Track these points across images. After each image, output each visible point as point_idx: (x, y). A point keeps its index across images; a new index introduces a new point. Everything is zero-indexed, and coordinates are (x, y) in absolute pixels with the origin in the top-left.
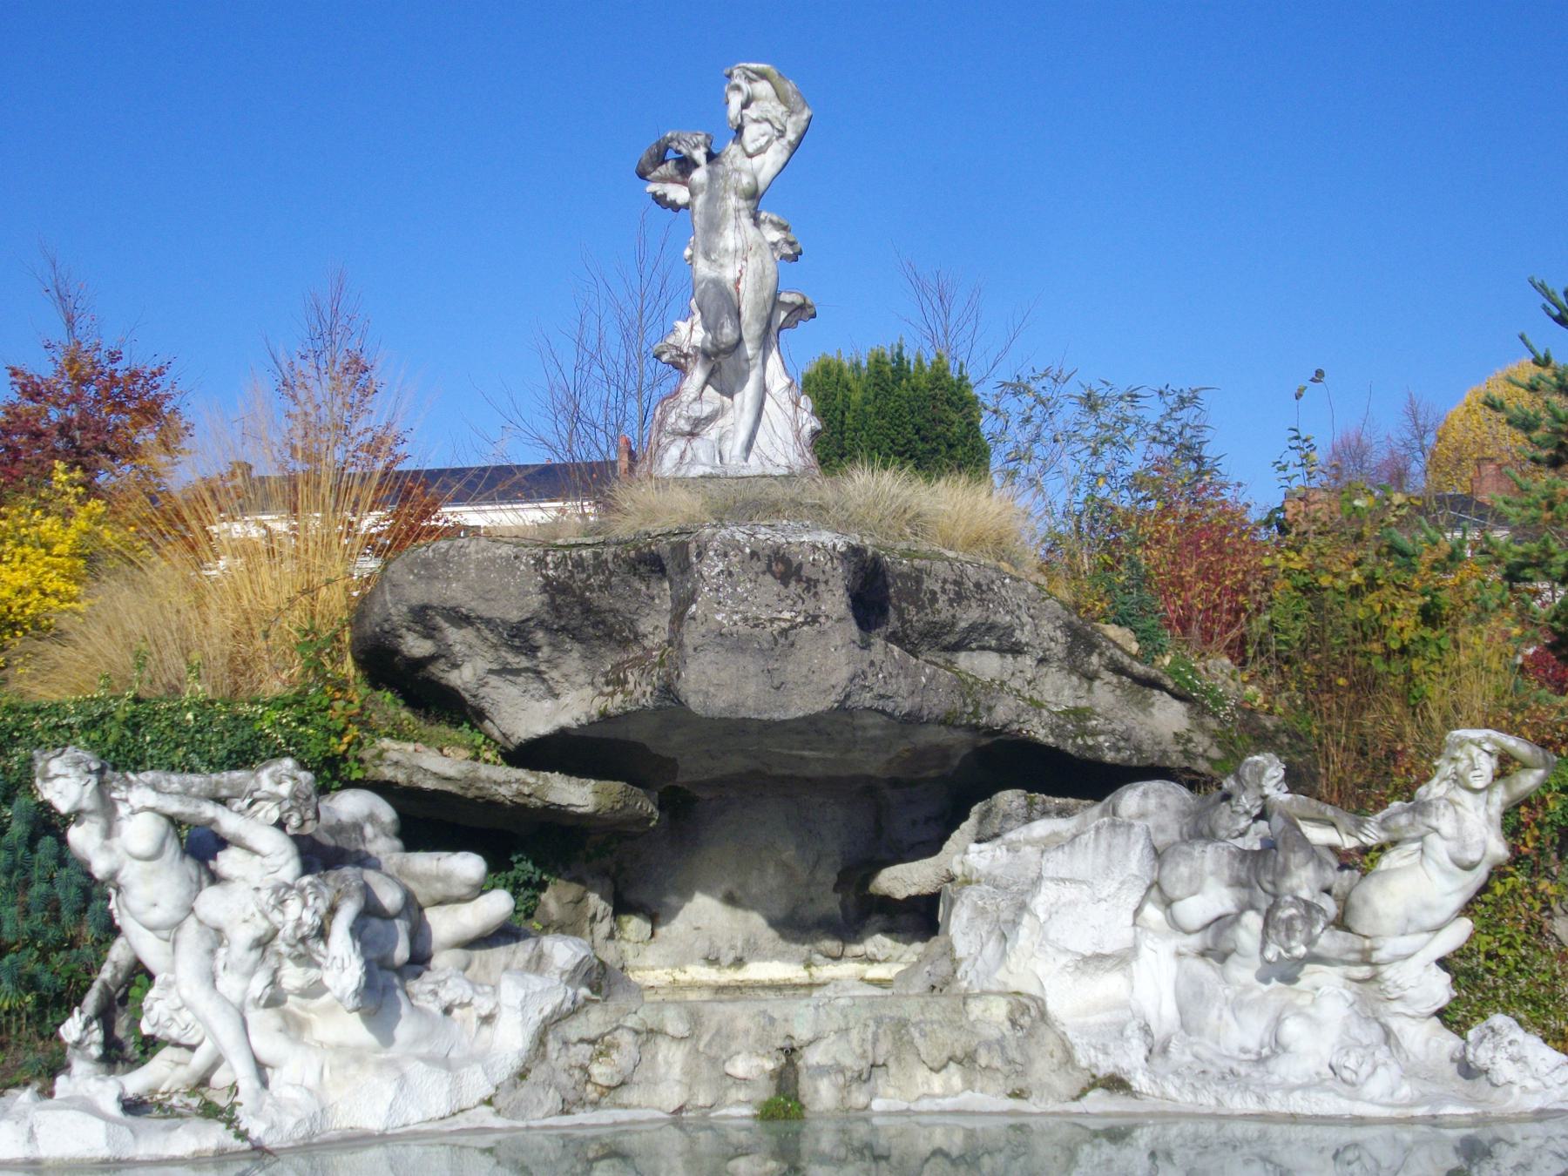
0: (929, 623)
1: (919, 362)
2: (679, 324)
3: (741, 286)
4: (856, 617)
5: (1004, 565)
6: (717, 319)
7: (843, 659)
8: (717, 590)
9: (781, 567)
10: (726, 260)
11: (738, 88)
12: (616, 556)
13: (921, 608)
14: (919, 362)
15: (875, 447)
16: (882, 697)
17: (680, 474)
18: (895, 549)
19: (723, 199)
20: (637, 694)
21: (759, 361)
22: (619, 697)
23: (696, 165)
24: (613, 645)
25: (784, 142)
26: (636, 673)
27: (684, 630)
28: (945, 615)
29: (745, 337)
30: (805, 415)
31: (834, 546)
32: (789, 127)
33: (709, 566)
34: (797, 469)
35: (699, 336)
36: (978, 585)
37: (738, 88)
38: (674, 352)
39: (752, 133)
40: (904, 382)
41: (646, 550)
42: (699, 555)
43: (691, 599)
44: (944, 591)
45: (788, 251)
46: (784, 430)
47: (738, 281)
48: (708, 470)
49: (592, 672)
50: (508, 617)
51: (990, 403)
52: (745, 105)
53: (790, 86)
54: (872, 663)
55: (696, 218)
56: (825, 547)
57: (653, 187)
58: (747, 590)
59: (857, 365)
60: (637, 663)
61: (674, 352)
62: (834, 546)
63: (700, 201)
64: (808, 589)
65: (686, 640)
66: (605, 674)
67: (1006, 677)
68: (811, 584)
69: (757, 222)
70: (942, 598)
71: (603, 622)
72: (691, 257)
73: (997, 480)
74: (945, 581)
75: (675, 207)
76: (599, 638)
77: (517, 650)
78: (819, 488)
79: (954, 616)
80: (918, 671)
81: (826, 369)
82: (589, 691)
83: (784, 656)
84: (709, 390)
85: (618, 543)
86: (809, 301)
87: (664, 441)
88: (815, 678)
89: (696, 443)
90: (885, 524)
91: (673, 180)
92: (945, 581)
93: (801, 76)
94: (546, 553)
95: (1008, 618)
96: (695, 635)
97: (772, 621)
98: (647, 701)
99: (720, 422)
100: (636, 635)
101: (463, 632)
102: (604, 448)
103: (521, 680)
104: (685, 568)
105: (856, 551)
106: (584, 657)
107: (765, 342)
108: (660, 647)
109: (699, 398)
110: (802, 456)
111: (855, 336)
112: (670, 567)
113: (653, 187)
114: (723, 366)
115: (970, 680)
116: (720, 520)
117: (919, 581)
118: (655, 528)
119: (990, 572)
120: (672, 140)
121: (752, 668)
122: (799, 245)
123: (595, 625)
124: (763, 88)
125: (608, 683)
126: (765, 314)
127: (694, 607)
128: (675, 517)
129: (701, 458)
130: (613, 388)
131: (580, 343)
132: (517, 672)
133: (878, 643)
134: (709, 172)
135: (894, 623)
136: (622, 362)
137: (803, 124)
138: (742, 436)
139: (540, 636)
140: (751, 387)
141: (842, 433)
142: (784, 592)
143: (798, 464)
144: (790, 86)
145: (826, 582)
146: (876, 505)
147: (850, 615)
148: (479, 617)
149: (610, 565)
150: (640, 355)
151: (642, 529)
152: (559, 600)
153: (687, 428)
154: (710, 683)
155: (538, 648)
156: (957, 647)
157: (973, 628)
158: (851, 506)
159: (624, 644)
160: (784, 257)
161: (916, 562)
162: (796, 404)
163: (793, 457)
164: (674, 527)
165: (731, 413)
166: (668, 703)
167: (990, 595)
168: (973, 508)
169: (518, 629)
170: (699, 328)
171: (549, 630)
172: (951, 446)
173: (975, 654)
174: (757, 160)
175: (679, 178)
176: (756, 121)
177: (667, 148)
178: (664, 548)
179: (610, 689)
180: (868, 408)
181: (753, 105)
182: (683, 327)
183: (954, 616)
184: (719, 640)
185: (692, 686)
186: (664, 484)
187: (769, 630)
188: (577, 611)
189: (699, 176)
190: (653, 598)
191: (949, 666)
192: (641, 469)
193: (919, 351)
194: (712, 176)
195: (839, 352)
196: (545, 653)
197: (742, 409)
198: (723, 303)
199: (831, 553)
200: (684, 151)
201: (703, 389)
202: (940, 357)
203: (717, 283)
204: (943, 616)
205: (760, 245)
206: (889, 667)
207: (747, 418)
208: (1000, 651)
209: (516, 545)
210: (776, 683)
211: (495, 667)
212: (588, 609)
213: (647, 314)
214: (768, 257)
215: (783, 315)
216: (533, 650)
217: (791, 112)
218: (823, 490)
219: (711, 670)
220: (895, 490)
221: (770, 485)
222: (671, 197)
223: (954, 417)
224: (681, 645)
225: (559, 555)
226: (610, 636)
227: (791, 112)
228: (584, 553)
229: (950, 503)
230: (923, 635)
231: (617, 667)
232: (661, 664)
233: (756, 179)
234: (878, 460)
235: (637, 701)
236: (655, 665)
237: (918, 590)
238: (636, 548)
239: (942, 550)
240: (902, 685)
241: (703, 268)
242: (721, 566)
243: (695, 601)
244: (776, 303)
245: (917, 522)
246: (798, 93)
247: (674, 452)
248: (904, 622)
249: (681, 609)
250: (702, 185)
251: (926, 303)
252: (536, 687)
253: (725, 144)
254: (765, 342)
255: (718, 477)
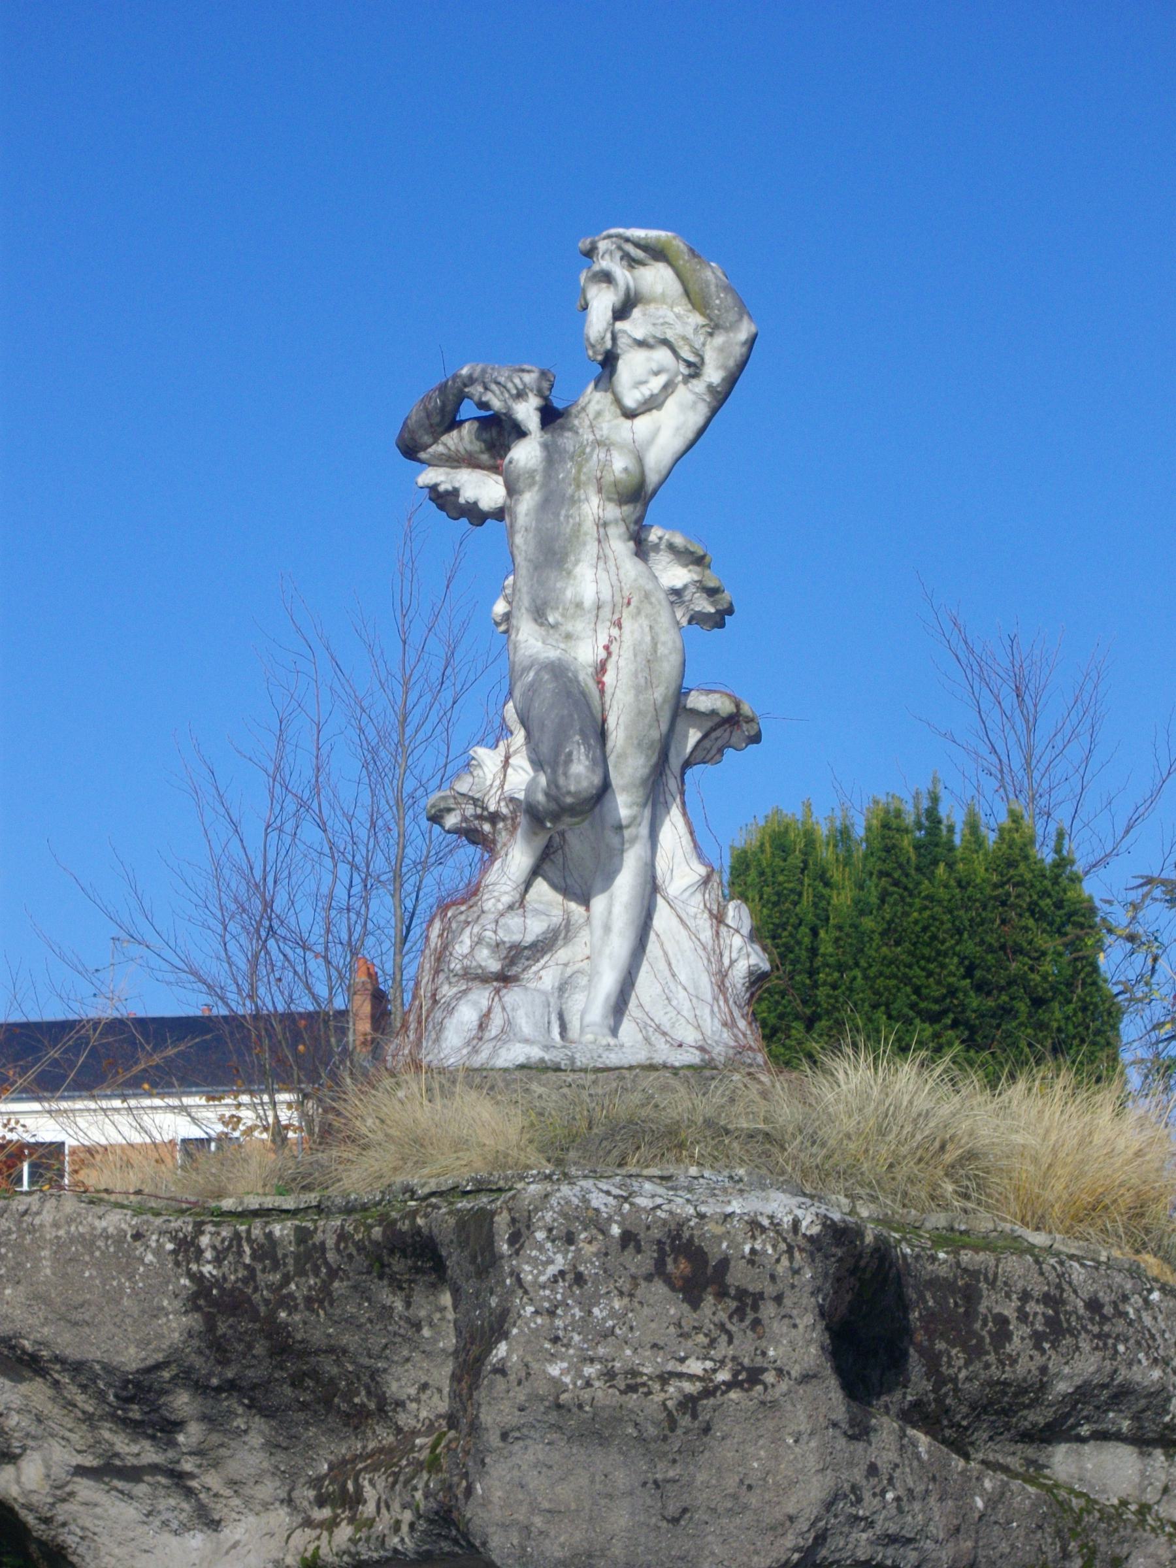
0: (991, 1383)
1: (973, 827)
2: (481, 752)
3: (608, 678)
4: (839, 1371)
5: (1150, 1262)
6: (558, 748)
7: (812, 1462)
8: (552, 1313)
9: (684, 1266)
10: (579, 626)
11: (607, 278)
12: (342, 1236)
13: (975, 1352)
14: (973, 827)
15: (881, 1002)
16: (892, 1539)
17: (478, 1060)
18: (919, 1226)
19: (574, 501)
20: (380, 1527)
21: (644, 830)
22: (344, 1532)
23: (520, 433)
24: (333, 1421)
25: (699, 386)
26: (381, 1483)
27: (481, 1395)
28: (1026, 1367)
29: (616, 780)
30: (737, 941)
31: (796, 1224)
32: (710, 356)
33: (534, 1262)
34: (719, 1053)
35: (521, 777)
36: (1094, 1305)
37: (607, 278)
38: (470, 810)
39: (637, 372)
40: (941, 869)
41: (405, 1226)
42: (514, 1239)
43: (498, 1329)
44: (1023, 1317)
45: (705, 606)
46: (693, 972)
47: (601, 668)
48: (535, 1053)
49: (290, 1477)
50: (117, 1360)
51: (1120, 917)
52: (621, 312)
53: (711, 274)
54: (873, 1470)
55: (519, 540)
56: (776, 1225)
57: (430, 476)
58: (613, 1314)
59: (844, 834)
60: (383, 1460)
61: (470, 810)
62: (796, 1224)
63: (527, 503)
64: (740, 1313)
65: (487, 1417)
66: (315, 1483)
67: (1150, 1496)
68: (747, 1303)
69: (642, 549)
70: (1019, 1333)
71: (314, 1374)
72: (507, 617)
73: (1135, 1078)
74: (1025, 1296)
75: (475, 515)
76: (304, 1406)
77: (136, 1429)
78: (764, 1095)
79: (1043, 1370)
80: (969, 1483)
81: (779, 841)
82: (281, 1517)
83: (690, 1452)
84: (541, 887)
85: (348, 1210)
86: (746, 709)
87: (447, 991)
88: (754, 1500)
89: (513, 996)
90: (901, 1173)
91: (471, 462)
92: (1025, 1296)
93: (735, 265)
94: (199, 1230)
95: (1156, 1374)
96: (506, 1406)
97: (664, 1378)
98: (405, 1542)
99: (562, 954)
100: (382, 1401)
101: (24, 1388)
102: (322, 991)
103: (141, 1489)
104: (486, 1262)
105: (839, 1234)
106: (272, 1447)
107: (656, 790)
108: (430, 1428)
109: (519, 904)
110: (729, 1024)
111: (836, 773)
112: (455, 1260)
113: (430, 476)
114: (570, 837)
115: (1076, 1503)
116: (559, 1162)
117: (971, 1296)
118: (425, 1179)
119: (1118, 1278)
120: (471, 380)
121: (622, 1479)
122: (727, 596)
123: (296, 1382)
124: (657, 278)
125: (321, 1502)
126: (655, 735)
127: (502, 1349)
128: (466, 1156)
129: (521, 1031)
130: (343, 869)
131: (277, 776)
132: (134, 1474)
133: (886, 1427)
134: (545, 446)
135: (918, 1384)
136: (362, 816)
137: (738, 351)
138: (608, 981)
139: (182, 1402)
140: (625, 883)
141: (812, 973)
142: (691, 1318)
143: (721, 1041)
144: (711, 274)
145: (778, 1299)
146: (882, 1132)
147: (828, 1370)
148: (57, 1359)
149: (331, 1256)
150: (399, 801)
151: (399, 1179)
152: (222, 1328)
153: (494, 966)
154: (534, 1508)
155: (178, 1425)
156: (1050, 1434)
157: (1083, 1393)
158: (831, 1135)
159: (357, 1420)
160: (696, 619)
161: (966, 1256)
162: (719, 918)
163: (712, 1026)
164: (462, 1176)
165: (584, 936)
166: (446, 1546)
167: (1120, 1326)
168: (1084, 1141)
169: (138, 1385)
170: (521, 761)
171: (200, 1388)
172: (1038, 1003)
173: (1086, 1448)
174: (643, 424)
175: (485, 458)
176: (642, 344)
177: (461, 397)
178: (440, 1221)
179: (326, 1512)
180: (868, 923)
181: (636, 313)
182: (488, 759)
183: (1043, 1370)
184: (553, 1417)
185: (497, 1514)
186: (446, 1081)
187: (658, 1397)
188: (259, 1349)
189: (526, 453)
190: (417, 1326)
191: (1035, 1471)
192: (398, 1048)
193: (973, 804)
194: (552, 455)
195: (808, 806)
196: (191, 1435)
197: (607, 929)
198: (568, 713)
199: (789, 1237)
200: (497, 404)
201: (528, 884)
202: (1016, 818)
203: (559, 671)
204: (1022, 1368)
205: (647, 596)
206: (908, 1478)
207: (619, 946)
208: (1141, 1441)
209: (138, 1211)
210: (672, 1509)
211: (89, 1461)
212: (283, 1346)
213: (414, 718)
214: (664, 619)
215: (694, 736)
216: (166, 1429)
217: (714, 327)
218: (775, 1099)
219: (534, 1481)
220: (922, 1102)
221: (664, 1088)
222: (468, 494)
223: (1045, 942)
224: (475, 1428)
225: (225, 1232)
226: (328, 1403)
227: (714, 327)
228: (277, 1229)
229: (1043, 1133)
230: (980, 1409)
231: (340, 1467)
232: (433, 1465)
233: (640, 461)
234: (889, 1033)
235: (382, 1540)
236: (419, 1466)
237: (970, 1314)
238: (383, 1219)
239: (1020, 1230)
240: (935, 1516)
241: (530, 641)
242: (560, 1262)
243: (505, 1335)
244: (679, 710)
245: (971, 1170)
246: (728, 289)
247: (466, 1014)
248: (941, 1381)
249: (475, 1350)
250: (531, 473)
251: (987, 701)
252: (172, 1504)
253: (581, 390)
254: (656, 790)
255: (558, 1069)
